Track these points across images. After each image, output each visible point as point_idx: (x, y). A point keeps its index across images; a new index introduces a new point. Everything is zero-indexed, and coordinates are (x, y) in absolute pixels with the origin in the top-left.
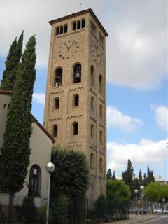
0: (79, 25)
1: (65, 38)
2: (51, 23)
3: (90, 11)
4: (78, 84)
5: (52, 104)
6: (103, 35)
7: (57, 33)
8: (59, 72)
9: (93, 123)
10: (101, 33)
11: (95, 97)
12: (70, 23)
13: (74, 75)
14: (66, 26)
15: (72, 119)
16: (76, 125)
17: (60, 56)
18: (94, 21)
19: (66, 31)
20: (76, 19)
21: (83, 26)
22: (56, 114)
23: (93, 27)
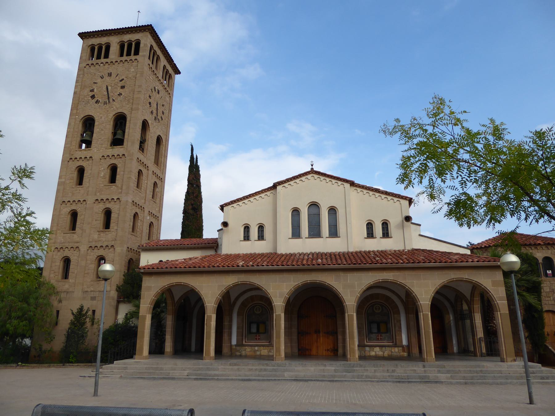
0: (130, 49)
1: (102, 67)
2: (83, 35)
8: (89, 123)
11: (144, 171)
12: (114, 42)
13: (114, 134)
16: (108, 213)
17: (93, 97)
19: (107, 56)
20: (127, 38)
21: (137, 53)
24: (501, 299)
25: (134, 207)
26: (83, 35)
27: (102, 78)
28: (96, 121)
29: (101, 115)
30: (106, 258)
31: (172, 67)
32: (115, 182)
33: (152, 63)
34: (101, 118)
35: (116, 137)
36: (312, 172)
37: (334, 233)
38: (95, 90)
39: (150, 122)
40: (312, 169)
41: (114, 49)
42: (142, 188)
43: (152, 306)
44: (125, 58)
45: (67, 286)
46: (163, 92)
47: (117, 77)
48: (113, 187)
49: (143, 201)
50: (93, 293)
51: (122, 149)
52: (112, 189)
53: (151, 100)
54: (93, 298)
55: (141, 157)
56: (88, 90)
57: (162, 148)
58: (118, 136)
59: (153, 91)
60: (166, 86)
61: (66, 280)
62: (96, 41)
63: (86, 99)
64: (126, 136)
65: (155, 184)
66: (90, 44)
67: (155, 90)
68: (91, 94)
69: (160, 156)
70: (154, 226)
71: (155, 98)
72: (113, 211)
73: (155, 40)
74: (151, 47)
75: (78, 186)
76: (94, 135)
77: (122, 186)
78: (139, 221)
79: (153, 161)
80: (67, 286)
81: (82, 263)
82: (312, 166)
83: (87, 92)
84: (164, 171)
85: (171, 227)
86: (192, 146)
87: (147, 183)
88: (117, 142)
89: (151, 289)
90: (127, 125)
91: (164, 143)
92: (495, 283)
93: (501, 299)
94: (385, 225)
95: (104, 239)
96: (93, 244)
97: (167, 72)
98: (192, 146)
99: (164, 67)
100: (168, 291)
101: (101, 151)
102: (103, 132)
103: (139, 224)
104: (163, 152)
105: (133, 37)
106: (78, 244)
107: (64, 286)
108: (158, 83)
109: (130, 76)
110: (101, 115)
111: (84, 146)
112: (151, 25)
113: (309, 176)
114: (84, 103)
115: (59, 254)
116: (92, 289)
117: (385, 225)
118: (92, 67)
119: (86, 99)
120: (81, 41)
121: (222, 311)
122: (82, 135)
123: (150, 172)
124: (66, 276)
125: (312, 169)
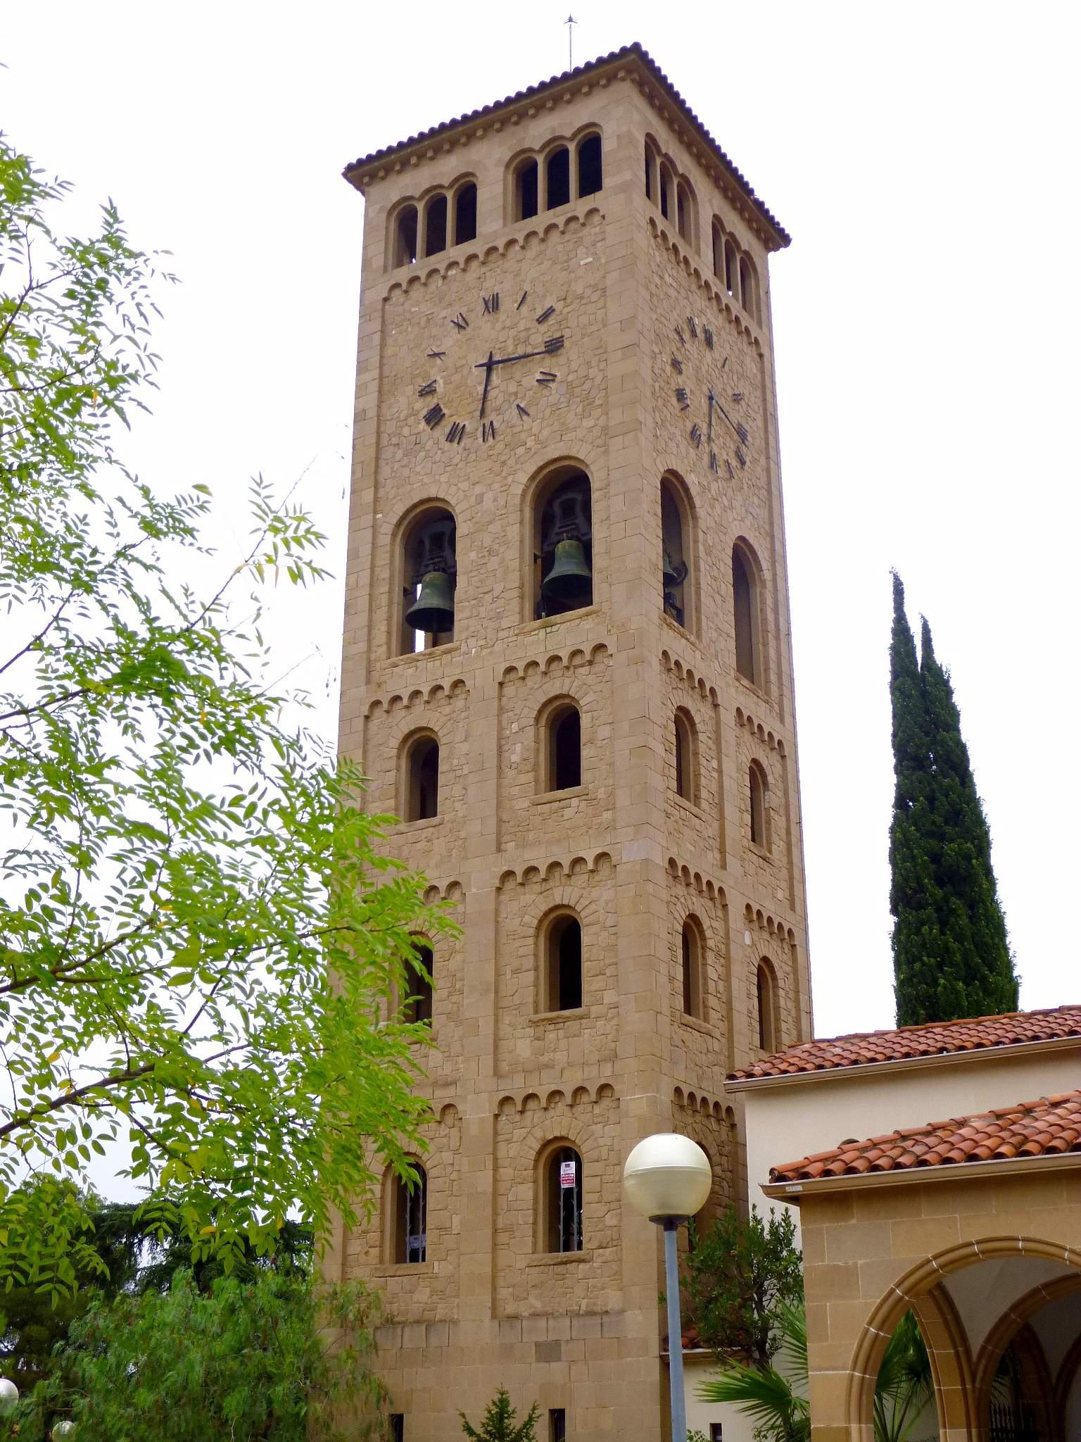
0: (563, 177)
1: (457, 278)
2: (362, 173)
3: (633, 68)
4: (560, 209)
5: (390, 775)
6: (747, 239)
7: (406, 248)
8: (428, 539)
9: (700, 906)
10: (735, 224)
11: (701, 713)
12: (490, 166)
13: (545, 560)
14: (467, 195)
15: (534, 679)
16: (564, 937)
17: (435, 416)
18: (669, 144)
19: (467, 231)
20: (536, 134)
21: (591, 183)
22: (426, 852)
23: (668, 190)
25: (680, 890)
27: (461, 325)
28: (459, 520)
29: (478, 489)
30: (585, 1150)
31: (749, 222)
32: (576, 781)
33: (664, 213)
35: (552, 575)
38: (440, 387)
39: (691, 480)
41: (494, 195)
42: (704, 794)
43: (871, 1378)
45: (423, 1295)
46: (725, 337)
47: (524, 309)
48: (571, 801)
49: (713, 857)
50: (542, 1323)
51: (588, 624)
52: (568, 813)
53: (680, 380)
54: (548, 1352)
55: (679, 648)
56: (410, 391)
57: (763, 596)
58: (562, 568)
59: (687, 336)
60: (736, 308)
61: (419, 1267)
64: (598, 561)
65: (757, 773)
66: (395, 198)
68: (423, 406)
69: (757, 638)
70: (778, 982)
71: (697, 370)
72: (584, 919)
73: (659, 110)
74: (651, 144)
75: (422, 823)
76: (461, 580)
77: (612, 794)
78: (710, 956)
79: (732, 661)
80: (423, 1295)
83: (406, 402)
84: (784, 707)
85: (852, 980)
87: (720, 771)
88: (561, 592)
89: (848, 1287)
90: (596, 508)
91: (767, 575)
95: (560, 1057)
97: (733, 245)
99: (718, 225)
100: (932, 1294)
101: (499, 646)
102: (494, 561)
103: (712, 973)
104: (770, 616)
105: (563, 123)
106: (451, 1091)
107: (410, 1292)
108: (699, 301)
110: (478, 489)
111: (420, 636)
112: (636, 46)
116: (538, 1305)
118: (417, 292)
119: (406, 431)
120: (354, 201)
122: (409, 593)
123: (728, 717)
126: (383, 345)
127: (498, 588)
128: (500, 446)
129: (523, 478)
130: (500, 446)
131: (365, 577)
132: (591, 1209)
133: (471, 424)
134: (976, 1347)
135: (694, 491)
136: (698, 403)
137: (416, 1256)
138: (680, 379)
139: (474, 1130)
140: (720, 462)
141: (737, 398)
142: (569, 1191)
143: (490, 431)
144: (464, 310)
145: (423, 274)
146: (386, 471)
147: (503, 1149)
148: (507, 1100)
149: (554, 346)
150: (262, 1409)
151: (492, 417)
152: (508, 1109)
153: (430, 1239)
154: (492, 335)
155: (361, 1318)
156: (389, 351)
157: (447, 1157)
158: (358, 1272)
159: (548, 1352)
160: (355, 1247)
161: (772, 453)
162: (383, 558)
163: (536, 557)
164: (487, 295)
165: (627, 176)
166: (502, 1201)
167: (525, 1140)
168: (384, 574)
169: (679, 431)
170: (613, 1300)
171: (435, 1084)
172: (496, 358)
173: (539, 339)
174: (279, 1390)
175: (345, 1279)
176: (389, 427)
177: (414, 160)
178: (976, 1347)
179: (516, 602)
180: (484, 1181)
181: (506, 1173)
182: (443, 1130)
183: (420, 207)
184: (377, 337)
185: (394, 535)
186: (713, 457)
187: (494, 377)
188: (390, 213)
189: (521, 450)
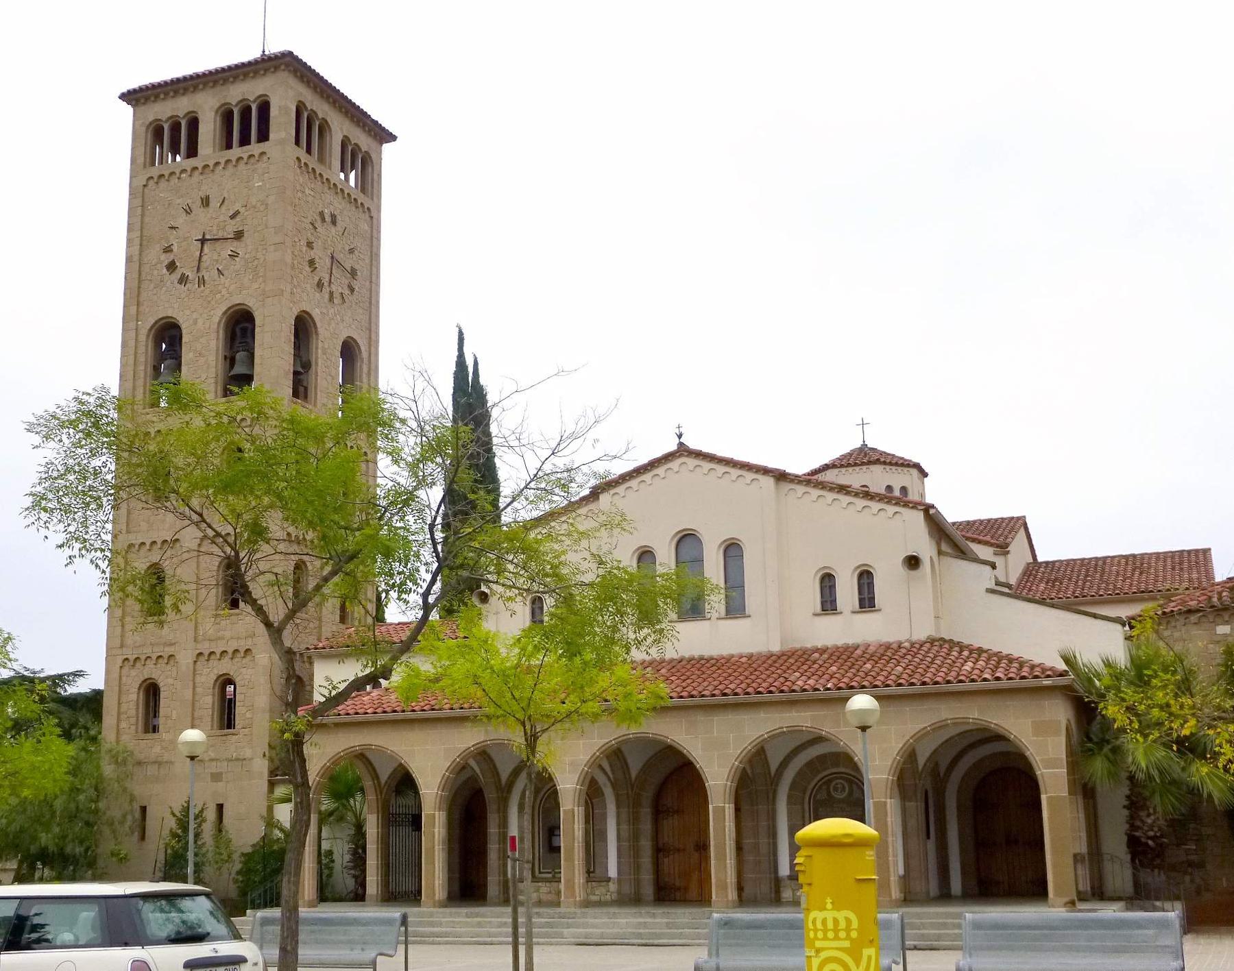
0: (247, 125)
2: (131, 97)
8: (167, 340)
12: (207, 107)
13: (231, 361)
20: (236, 93)
21: (264, 136)
23: (309, 130)
24: (1050, 763)
26: (131, 97)
27: (188, 211)
29: (195, 316)
30: (237, 680)
33: (309, 151)
34: (195, 322)
36: (683, 451)
37: (735, 609)
38: (175, 248)
39: (316, 313)
40: (681, 444)
41: (208, 130)
44: (236, 152)
45: (157, 749)
47: (224, 208)
50: (214, 763)
53: (312, 254)
54: (216, 777)
58: (239, 369)
61: (155, 735)
62: (163, 110)
63: (155, 272)
66: (151, 118)
67: (323, 220)
80: (157, 749)
81: (185, 690)
82: (680, 436)
83: (155, 254)
86: (461, 335)
88: (238, 378)
92: (1041, 729)
93: (1050, 763)
94: (865, 578)
95: (228, 634)
96: (206, 648)
98: (461, 335)
102: (202, 360)
105: (249, 90)
109: (253, 201)
110: (195, 316)
113: (675, 464)
114: (152, 286)
115: (133, 673)
117: (865, 578)
119: (155, 272)
120: (127, 110)
121: (591, 794)
124: (151, 726)
125: (681, 444)
126: (143, 215)
127: (204, 376)
128: (207, 292)
129: (219, 312)
130: (207, 292)
131: (131, 361)
132: (239, 710)
133: (191, 274)
134: (383, 782)
135: (317, 320)
136: (323, 263)
137: (155, 729)
138: (312, 253)
139: (184, 668)
140: (336, 295)
141: (351, 251)
142: (230, 700)
143: (202, 282)
144: (189, 201)
145: (166, 173)
146: (144, 295)
147: (198, 679)
148: (200, 654)
149: (239, 235)
150: (73, 806)
151: (203, 273)
152: (201, 658)
153: (161, 721)
154: (207, 222)
155: (125, 762)
156: (147, 220)
157: (170, 681)
158: (125, 738)
159: (216, 777)
160: (123, 725)
161: (374, 278)
162: (142, 349)
163: (226, 357)
164: (202, 194)
165: (283, 135)
166: (197, 704)
167: (208, 675)
168: (142, 359)
169: (309, 286)
170: (248, 753)
171: (165, 644)
172: (207, 237)
173: (232, 227)
174: (82, 797)
175: (118, 742)
176: (146, 269)
177: (162, 96)
178: (383, 782)
179: (213, 386)
180: (188, 694)
181: (199, 690)
182: (169, 667)
183: (166, 127)
184: (139, 210)
185: (148, 336)
186: (331, 294)
187: (205, 247)
188: (148, 127)
189: (218, 296)
